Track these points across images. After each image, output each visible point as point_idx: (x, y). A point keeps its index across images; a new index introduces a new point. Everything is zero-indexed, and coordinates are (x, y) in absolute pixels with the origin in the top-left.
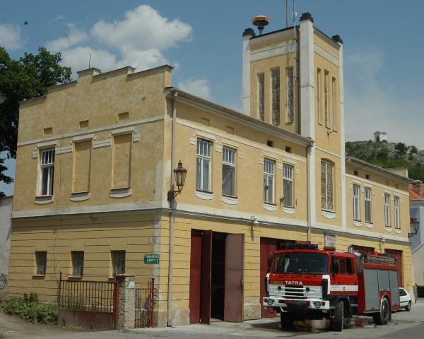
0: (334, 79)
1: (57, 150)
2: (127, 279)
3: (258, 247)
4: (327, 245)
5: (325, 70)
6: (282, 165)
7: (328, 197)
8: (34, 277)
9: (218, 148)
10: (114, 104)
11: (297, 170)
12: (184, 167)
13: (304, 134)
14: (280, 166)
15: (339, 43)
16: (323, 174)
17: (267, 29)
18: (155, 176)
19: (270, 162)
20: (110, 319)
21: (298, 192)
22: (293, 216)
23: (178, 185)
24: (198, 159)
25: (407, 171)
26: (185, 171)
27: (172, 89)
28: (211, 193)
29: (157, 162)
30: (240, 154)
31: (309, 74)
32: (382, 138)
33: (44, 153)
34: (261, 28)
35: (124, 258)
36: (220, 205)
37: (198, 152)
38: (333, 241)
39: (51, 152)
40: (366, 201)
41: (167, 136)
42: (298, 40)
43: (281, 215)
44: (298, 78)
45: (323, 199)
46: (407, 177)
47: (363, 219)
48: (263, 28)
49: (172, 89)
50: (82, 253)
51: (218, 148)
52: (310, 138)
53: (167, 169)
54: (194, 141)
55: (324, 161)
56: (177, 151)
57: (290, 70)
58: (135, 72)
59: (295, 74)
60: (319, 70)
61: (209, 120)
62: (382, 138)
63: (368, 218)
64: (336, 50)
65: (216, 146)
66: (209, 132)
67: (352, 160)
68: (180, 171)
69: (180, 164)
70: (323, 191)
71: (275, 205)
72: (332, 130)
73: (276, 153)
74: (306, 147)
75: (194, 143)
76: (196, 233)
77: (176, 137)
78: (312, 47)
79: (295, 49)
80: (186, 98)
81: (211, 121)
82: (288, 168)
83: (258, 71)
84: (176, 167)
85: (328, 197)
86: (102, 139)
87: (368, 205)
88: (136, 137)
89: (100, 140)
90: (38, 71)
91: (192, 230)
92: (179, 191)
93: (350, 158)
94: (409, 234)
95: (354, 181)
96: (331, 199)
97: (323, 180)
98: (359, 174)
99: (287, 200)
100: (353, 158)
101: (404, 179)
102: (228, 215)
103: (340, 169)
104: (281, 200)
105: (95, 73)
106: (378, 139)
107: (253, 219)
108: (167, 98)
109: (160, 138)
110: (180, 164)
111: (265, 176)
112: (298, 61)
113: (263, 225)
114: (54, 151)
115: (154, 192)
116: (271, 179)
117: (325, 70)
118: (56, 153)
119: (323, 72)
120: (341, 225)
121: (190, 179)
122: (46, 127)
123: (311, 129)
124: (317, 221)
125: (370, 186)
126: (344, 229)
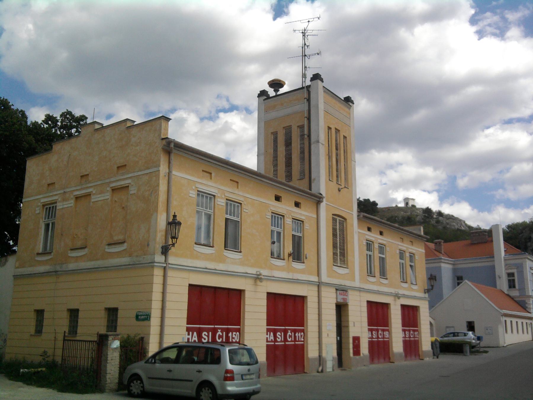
0: (345, 137)
1: (59, 206)
2: (110, 338)
3: (264, 302)
4: (339, 300)
5: (336, 129)
6: (291, 220)
7: (340, 253)
8: (31, 335)
9: (288, 221)
10: (114, 157)
11: (307, 226)
12: (178, 219)
13: (314, 191)
14: (288, 221)
15: (351, 104)
16: (334, 230)
17: (282, 91)
18: (149, 229)
19: (278, 218)
20: (92, 380)
21: (308, 249)
22: (302, 272)
23: (173, 238)
24: (272, 231)
25: (422, 228)
26: (179, 224)
27: (167, 140)
28: (212, 247)
29: (152, 215)
30: (247, 209)
31: (320, 133)
32: (411, 203)
33: (47, 208)
34: (276, 91)
35: (117, 315)
36: (222, 260)
37: (272, 226)
38: (345, 297)
39: (53, 207)
40: (380, 257)
41: (163, 188)
42: (309, 100)
43: (290, 269)
44: (309, 136)
45: (335, 254)
46: (422, 233)
47: (377, 274)
48: (278, 91)
49: (167, 140)
50: (78, 310)
51: (221, 202)
52: (321, 194)
53: (162, 221)
54: (193, 194)
55: (335, 216)
56: (174, 203)
57: (301, 127)
58: (135, 123)
59: (306, 132)
60: (329, 128)
61: (211, 174)
62: (411, 203)
63: (383, 274)
64: (347, 109)
65: (219, 200)
66: (210, 186)
67: (364, 217)
68: (174, 224)
69: (175, 216)
70: (335, 246)
71: (284, 259)
72: (343, 186)
73: (285, 207)
74: (318, 200)
75: (194, 196)
76: (370, 304)
77: (173, 189)
78: (321, 106)
79: (306, 108)
80: (182, 148)
81: (213, 175)
82: (299, 222)
83: (272, 130)
84: (171, 220)
85: (340, 253)
86: (101, 192)
87: (382, 261)
88: (133, 190)
89: (100, 194)
90: (56, 130)
91: (190, 285)
92: (173, 245)
93: (362, 214)
94: (425, 290)
95: (367, 237)
96: (344, 256)
97: (334, 235)
98: (302, 206)
99: (297, 255)
100: (366, 214)
101: (420, 236)
102: (230, 269)
103: (352, 225)
104: (290, 255)
105: (97, 126)
106: (407, 204)
107: (258, 273)
108: (163, 149)
109: (155, 189)
110: (175, 216)
111: (272, 231)
112: (309, 119)
113: (404, 296)
114: (56, 206)
115: (148, 245)
116: (279, 234)
117: (336, 129)
118: (58, 208)
119: (333, 131)
120: (355, 281)
121: (186, 233)
122: (49, 182)
123: (323, 184)
124: (328, 276)
125: (384, 242)
126: (357, 283)
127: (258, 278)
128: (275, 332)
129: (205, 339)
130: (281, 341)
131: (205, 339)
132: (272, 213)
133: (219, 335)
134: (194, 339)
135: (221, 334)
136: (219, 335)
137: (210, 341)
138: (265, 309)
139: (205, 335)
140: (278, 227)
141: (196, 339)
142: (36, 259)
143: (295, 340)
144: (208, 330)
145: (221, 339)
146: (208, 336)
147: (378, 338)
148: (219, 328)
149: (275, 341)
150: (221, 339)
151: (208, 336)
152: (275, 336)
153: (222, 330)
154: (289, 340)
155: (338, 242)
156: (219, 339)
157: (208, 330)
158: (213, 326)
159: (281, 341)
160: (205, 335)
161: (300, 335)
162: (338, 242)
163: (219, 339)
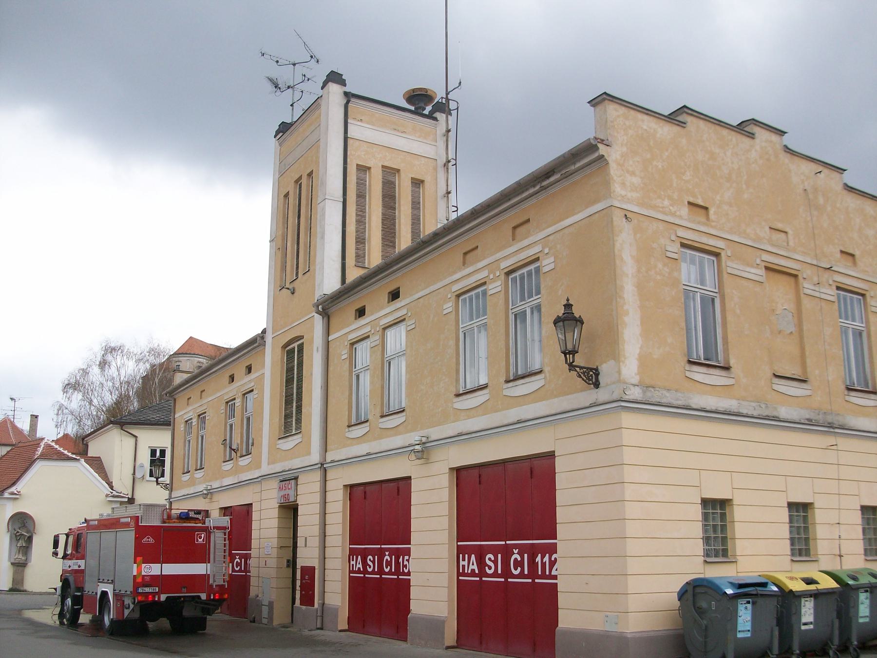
111: (844, 331)
127: (423, 451)
128: (364, 554)
129: (490, 568)
130: (495, 575)
131: (490, 568)
132: (838, 288)
133: (516, 559)
134: (471, 567)
135: (519, 559)
136: (516, 559)
137: (500, 572)
138: (414, 512)
139: (490, 559)
140: (854, 320)
141: (475, 567)
142: (506, 392)
143: (533, 574)
144: (494, 550)
145: (519, 569)
146: (495, 562)
147: (381, 571)
148: (516, 546)
149: (482, 573)
150: (519, 569)
151: (373, 562)
152: (481, 563)
153: (522, 550)
154: (387, 570)
155: (295, 391)
156: (516, 569)
157: (494, 550)
158: (503, 543)
159: (495, 575)
160: (490, 559)
161: (546, 559)
162: (295, 391)
163: (516, 569)
